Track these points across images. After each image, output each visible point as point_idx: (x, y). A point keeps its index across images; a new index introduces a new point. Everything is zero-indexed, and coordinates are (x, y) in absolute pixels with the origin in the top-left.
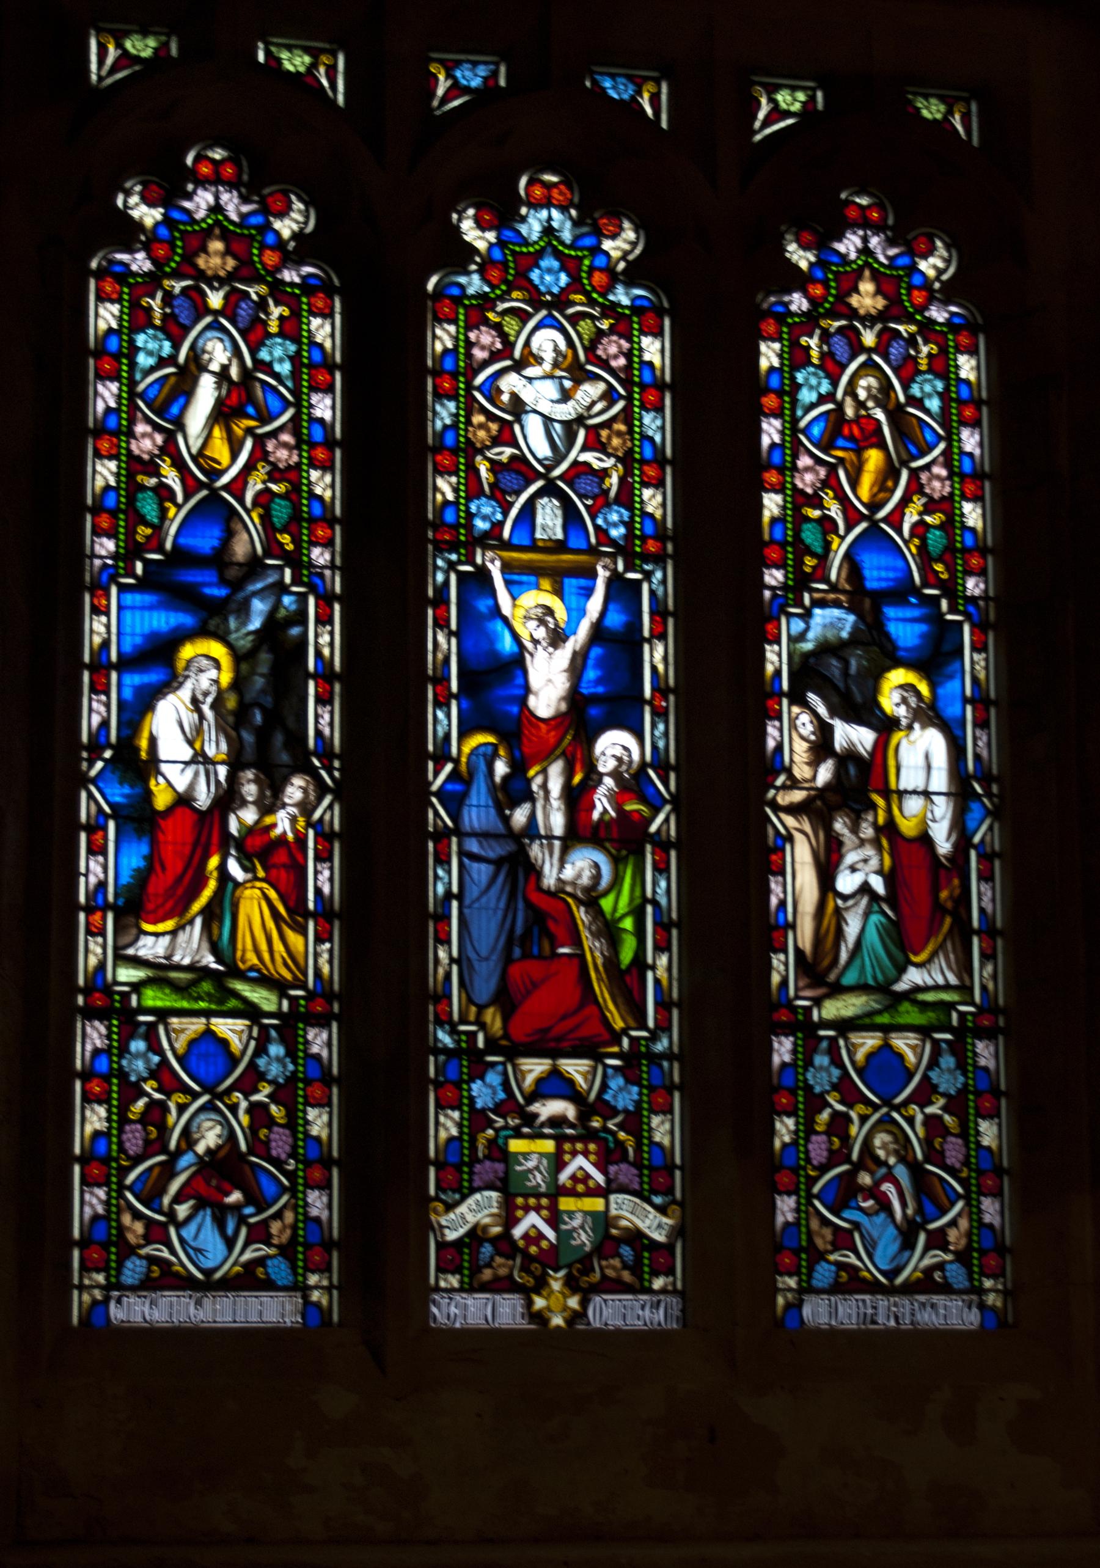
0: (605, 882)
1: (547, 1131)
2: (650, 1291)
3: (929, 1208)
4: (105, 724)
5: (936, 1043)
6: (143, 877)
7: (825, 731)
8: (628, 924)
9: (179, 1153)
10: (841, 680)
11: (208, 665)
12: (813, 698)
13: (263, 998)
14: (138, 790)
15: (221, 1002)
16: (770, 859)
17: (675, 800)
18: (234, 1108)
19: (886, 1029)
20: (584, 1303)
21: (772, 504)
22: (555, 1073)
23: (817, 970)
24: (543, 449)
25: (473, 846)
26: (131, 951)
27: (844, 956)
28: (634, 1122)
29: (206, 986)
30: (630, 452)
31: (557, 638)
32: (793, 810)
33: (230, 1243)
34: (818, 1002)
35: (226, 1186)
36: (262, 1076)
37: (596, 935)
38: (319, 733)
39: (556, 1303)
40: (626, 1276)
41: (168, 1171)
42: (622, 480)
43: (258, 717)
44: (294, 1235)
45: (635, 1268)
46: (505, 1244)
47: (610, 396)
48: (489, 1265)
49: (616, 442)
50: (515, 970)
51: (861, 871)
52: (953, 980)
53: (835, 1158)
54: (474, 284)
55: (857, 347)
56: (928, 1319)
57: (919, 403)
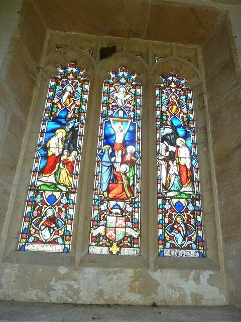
0: (128, 171)
1: (114, 215)
2: (133, 247)
3: (188, 232)
4: (42, 142)
5: (188, 201)
6: (44, 167)
7: (167, 147)
8: (132, 178)
9: (44, 216)
10: (170, 140)
11: (61, 134)
12: (165, 142)
13: (64, 189)
14: (46, 152)
15: (55, 189)
16: (157, 168)
17: (141, 158)
18: (55, 208)
19: (179, 198)
20: (120, 249)
21: (158, 113)
22: (117, 204)
23: (166, 187)
24: (121, 104)
25: (104, 163)
26: (40, 179)
27: (171, 185)
28: (132, 214)
29: (53, 186)
30: (134, 105)
31: (121, 131)
32: (162, 160)
33: (51, 234)
34: (166, 193)
35: (52, 223)
36: (61, 203)
37: (126, 180)
38: (79, 145)
39: (115, 249)
40: (129, 244)
41: (41, 220)
42: (133, 109)
43: (69, 142)
44: (64, 233)
45: (131, 243)
46: (105, 237)
47: (132, 97)
48: (101, 241)
49: (133, 103)
50: (110, 185)
51: (174, 169)
52: (191, 190)
53: (170, 222)
54: (111, 81)
55: (171, 92)
56: (188, 255)
57: (182, 100)
